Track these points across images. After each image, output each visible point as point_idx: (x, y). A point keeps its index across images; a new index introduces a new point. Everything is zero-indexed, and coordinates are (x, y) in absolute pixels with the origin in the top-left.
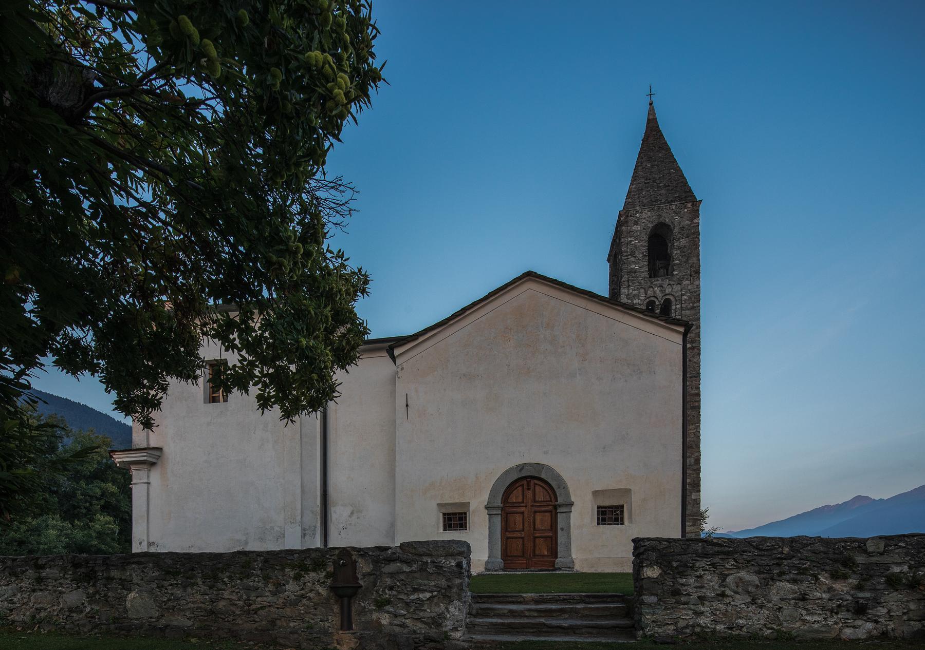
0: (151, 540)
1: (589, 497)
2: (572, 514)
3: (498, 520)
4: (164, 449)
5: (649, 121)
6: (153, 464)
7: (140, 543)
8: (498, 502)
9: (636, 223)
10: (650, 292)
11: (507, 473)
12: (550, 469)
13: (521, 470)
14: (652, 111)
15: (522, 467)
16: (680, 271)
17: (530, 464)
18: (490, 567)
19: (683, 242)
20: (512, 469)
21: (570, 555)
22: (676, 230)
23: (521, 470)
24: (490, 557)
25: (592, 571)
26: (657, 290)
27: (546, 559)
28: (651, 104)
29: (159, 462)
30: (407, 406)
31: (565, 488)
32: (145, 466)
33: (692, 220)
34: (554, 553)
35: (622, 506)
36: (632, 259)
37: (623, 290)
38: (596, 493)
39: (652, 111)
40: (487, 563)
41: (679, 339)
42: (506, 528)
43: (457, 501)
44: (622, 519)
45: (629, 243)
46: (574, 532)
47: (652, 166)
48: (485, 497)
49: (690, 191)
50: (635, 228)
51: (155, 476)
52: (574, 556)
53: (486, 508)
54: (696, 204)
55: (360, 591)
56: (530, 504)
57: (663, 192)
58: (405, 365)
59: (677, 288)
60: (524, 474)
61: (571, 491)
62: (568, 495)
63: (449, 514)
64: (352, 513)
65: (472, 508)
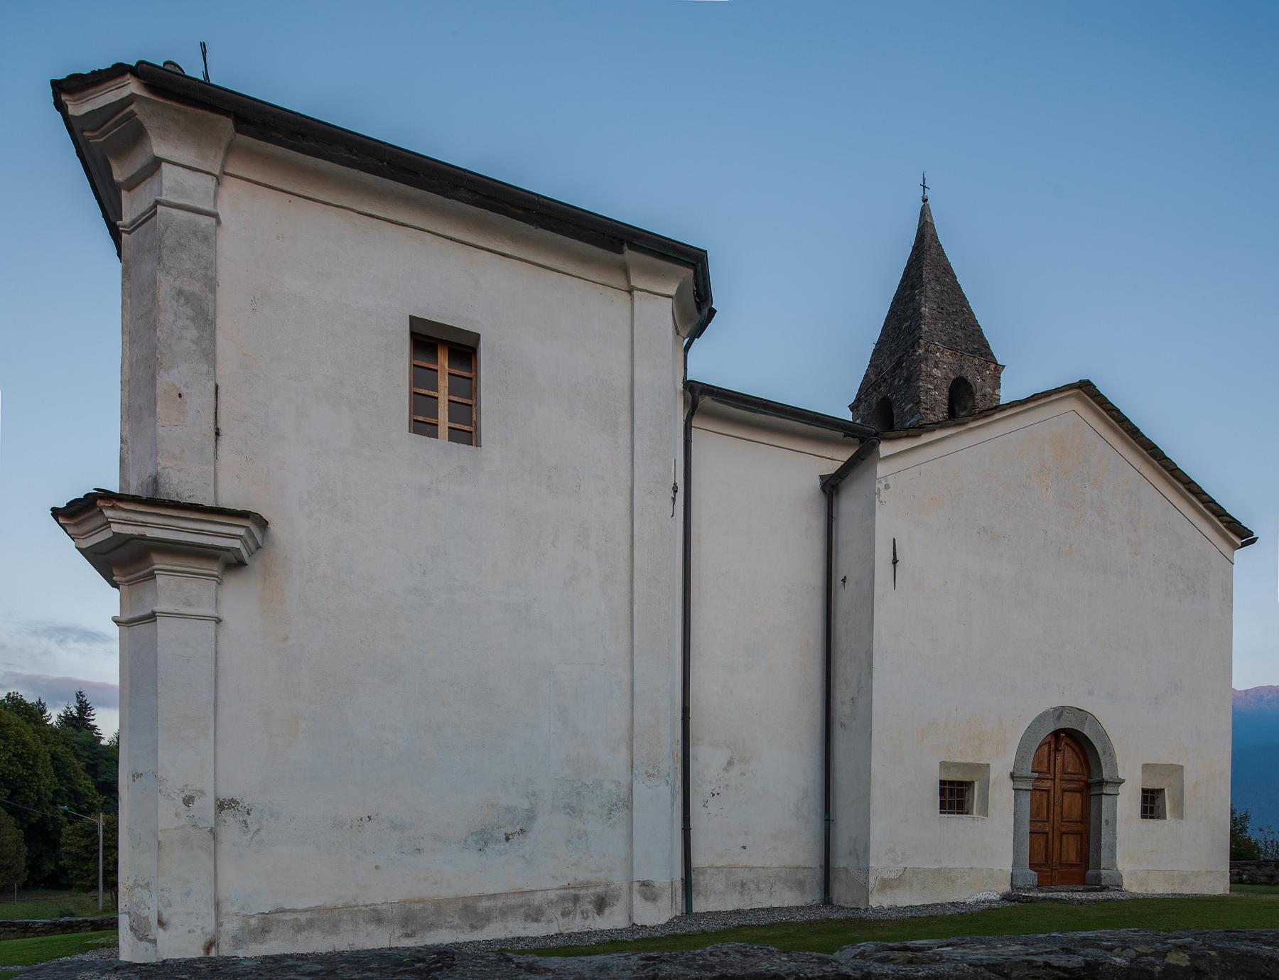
0: (226, 794)
2: (1119, 798)
6: (234, 564)
7: (188, 801)
8: (1027, 770)
11: (1040, 719)
13: (1059, 717)
14: (925, 212)
18: (1019, 883)
20: (1046, 713)
21: (1114, 865)
23: (1059, 717)
27: (1074, 869)
28: (925, 201)
29: (255, 564)
30: (895, 562)
32: (215, 569)
35: (970, 784)
38: (944, 765)
39: (925, 212)
43: (972, 761)
50: (935, 371)
51: (238, 600)
52: (1120, 867)
54: (999, 368)
55: (24, 878)
56: (1058, 775)
58: (891, 480)
61: (1118, 759)
63: (951, 783)
64: (730, 763)
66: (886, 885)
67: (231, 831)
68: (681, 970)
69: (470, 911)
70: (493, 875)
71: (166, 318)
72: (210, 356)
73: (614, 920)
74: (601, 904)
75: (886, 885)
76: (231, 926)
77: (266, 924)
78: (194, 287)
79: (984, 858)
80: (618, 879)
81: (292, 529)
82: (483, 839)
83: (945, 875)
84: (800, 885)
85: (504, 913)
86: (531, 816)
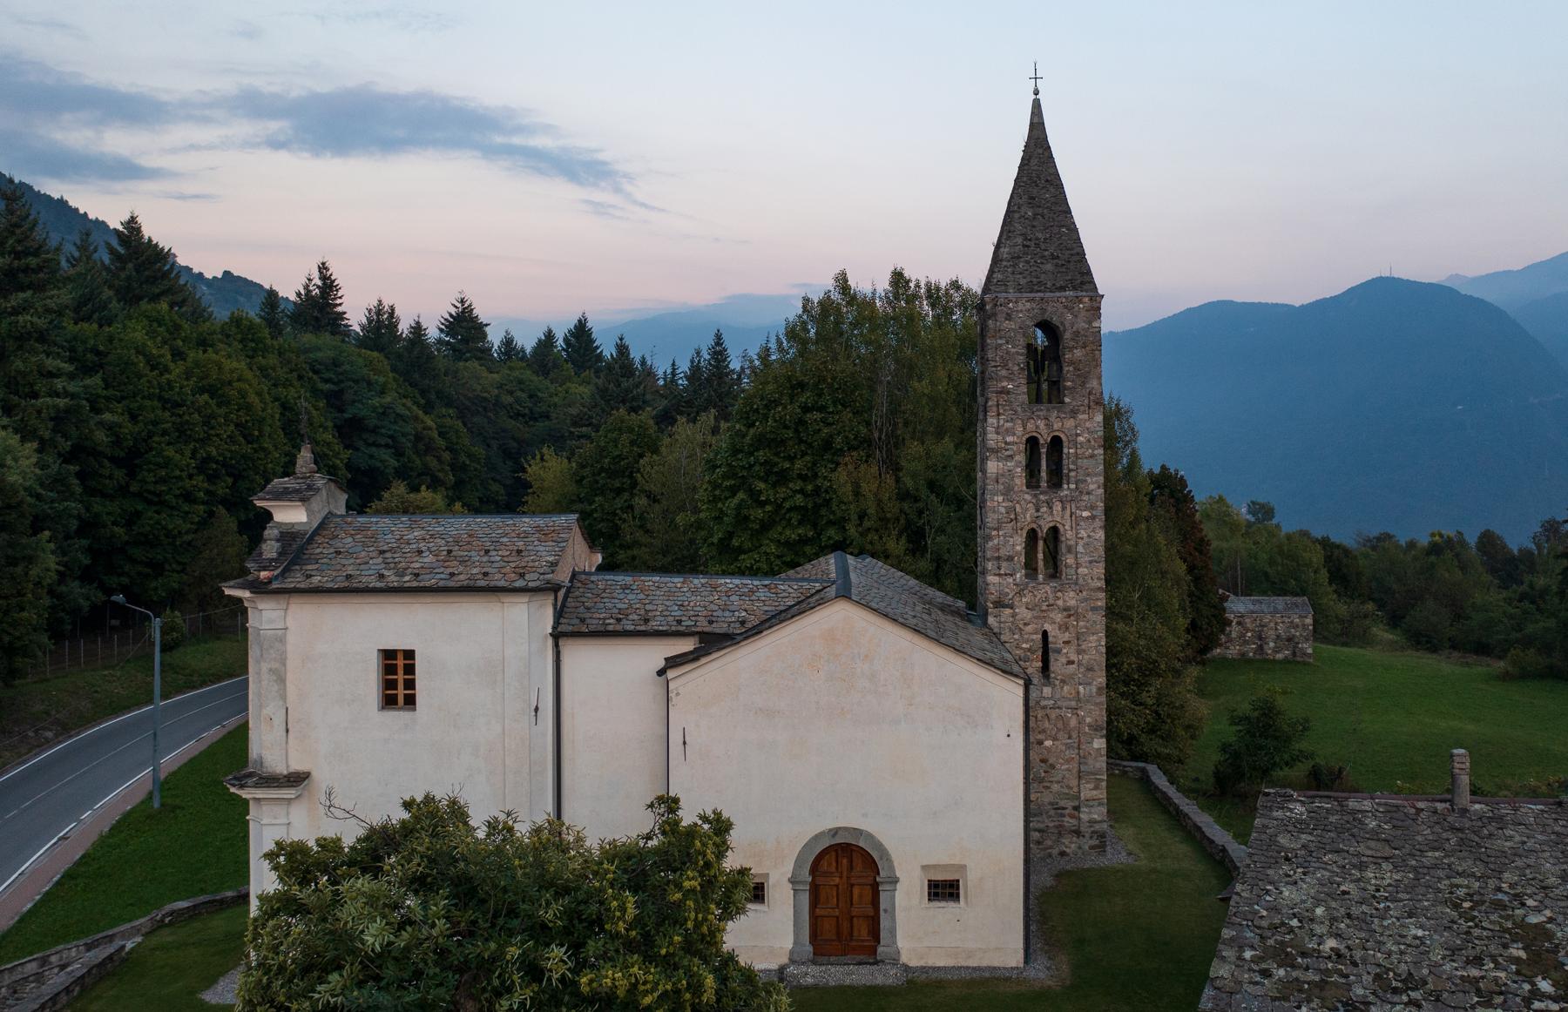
1: (918, 872)
3: (805, 898)
4: (314, 774)
5: (1032, 125)
9: (1009, 317)
10: (1030, 426)
11: (817, 838)
12: (870, 836)
13: (834, 836)
14: (1037, 106)
15: (835, 832)
16: (1073, 399)
17: (846, 829)
19: (1078, 353)
22: (1067, 335)
24: (795, 943)
25: (922, 963)
26: (1041, 423)
31: (889, 860)
33: (1090, 323)
34: (877, 938)
36: (1004, 373)
37: (990, 420)
38: (925, 868)
39: (1037, 106)
40: (792, 952)
41: (1020, 691)
42: (814, 903)
44: (958, 896)
45: (998, 347)
46: (900, 915)
47: (1035, 215)
48: (788, 868)
49: (1089, 273)
52: (900, 944)
53: (791, 881)
57: (1049, 267)
59: (1070, 423)
60: (838, 840)
62: (892, 868)
65: (772, 881)
81: (323, 776)
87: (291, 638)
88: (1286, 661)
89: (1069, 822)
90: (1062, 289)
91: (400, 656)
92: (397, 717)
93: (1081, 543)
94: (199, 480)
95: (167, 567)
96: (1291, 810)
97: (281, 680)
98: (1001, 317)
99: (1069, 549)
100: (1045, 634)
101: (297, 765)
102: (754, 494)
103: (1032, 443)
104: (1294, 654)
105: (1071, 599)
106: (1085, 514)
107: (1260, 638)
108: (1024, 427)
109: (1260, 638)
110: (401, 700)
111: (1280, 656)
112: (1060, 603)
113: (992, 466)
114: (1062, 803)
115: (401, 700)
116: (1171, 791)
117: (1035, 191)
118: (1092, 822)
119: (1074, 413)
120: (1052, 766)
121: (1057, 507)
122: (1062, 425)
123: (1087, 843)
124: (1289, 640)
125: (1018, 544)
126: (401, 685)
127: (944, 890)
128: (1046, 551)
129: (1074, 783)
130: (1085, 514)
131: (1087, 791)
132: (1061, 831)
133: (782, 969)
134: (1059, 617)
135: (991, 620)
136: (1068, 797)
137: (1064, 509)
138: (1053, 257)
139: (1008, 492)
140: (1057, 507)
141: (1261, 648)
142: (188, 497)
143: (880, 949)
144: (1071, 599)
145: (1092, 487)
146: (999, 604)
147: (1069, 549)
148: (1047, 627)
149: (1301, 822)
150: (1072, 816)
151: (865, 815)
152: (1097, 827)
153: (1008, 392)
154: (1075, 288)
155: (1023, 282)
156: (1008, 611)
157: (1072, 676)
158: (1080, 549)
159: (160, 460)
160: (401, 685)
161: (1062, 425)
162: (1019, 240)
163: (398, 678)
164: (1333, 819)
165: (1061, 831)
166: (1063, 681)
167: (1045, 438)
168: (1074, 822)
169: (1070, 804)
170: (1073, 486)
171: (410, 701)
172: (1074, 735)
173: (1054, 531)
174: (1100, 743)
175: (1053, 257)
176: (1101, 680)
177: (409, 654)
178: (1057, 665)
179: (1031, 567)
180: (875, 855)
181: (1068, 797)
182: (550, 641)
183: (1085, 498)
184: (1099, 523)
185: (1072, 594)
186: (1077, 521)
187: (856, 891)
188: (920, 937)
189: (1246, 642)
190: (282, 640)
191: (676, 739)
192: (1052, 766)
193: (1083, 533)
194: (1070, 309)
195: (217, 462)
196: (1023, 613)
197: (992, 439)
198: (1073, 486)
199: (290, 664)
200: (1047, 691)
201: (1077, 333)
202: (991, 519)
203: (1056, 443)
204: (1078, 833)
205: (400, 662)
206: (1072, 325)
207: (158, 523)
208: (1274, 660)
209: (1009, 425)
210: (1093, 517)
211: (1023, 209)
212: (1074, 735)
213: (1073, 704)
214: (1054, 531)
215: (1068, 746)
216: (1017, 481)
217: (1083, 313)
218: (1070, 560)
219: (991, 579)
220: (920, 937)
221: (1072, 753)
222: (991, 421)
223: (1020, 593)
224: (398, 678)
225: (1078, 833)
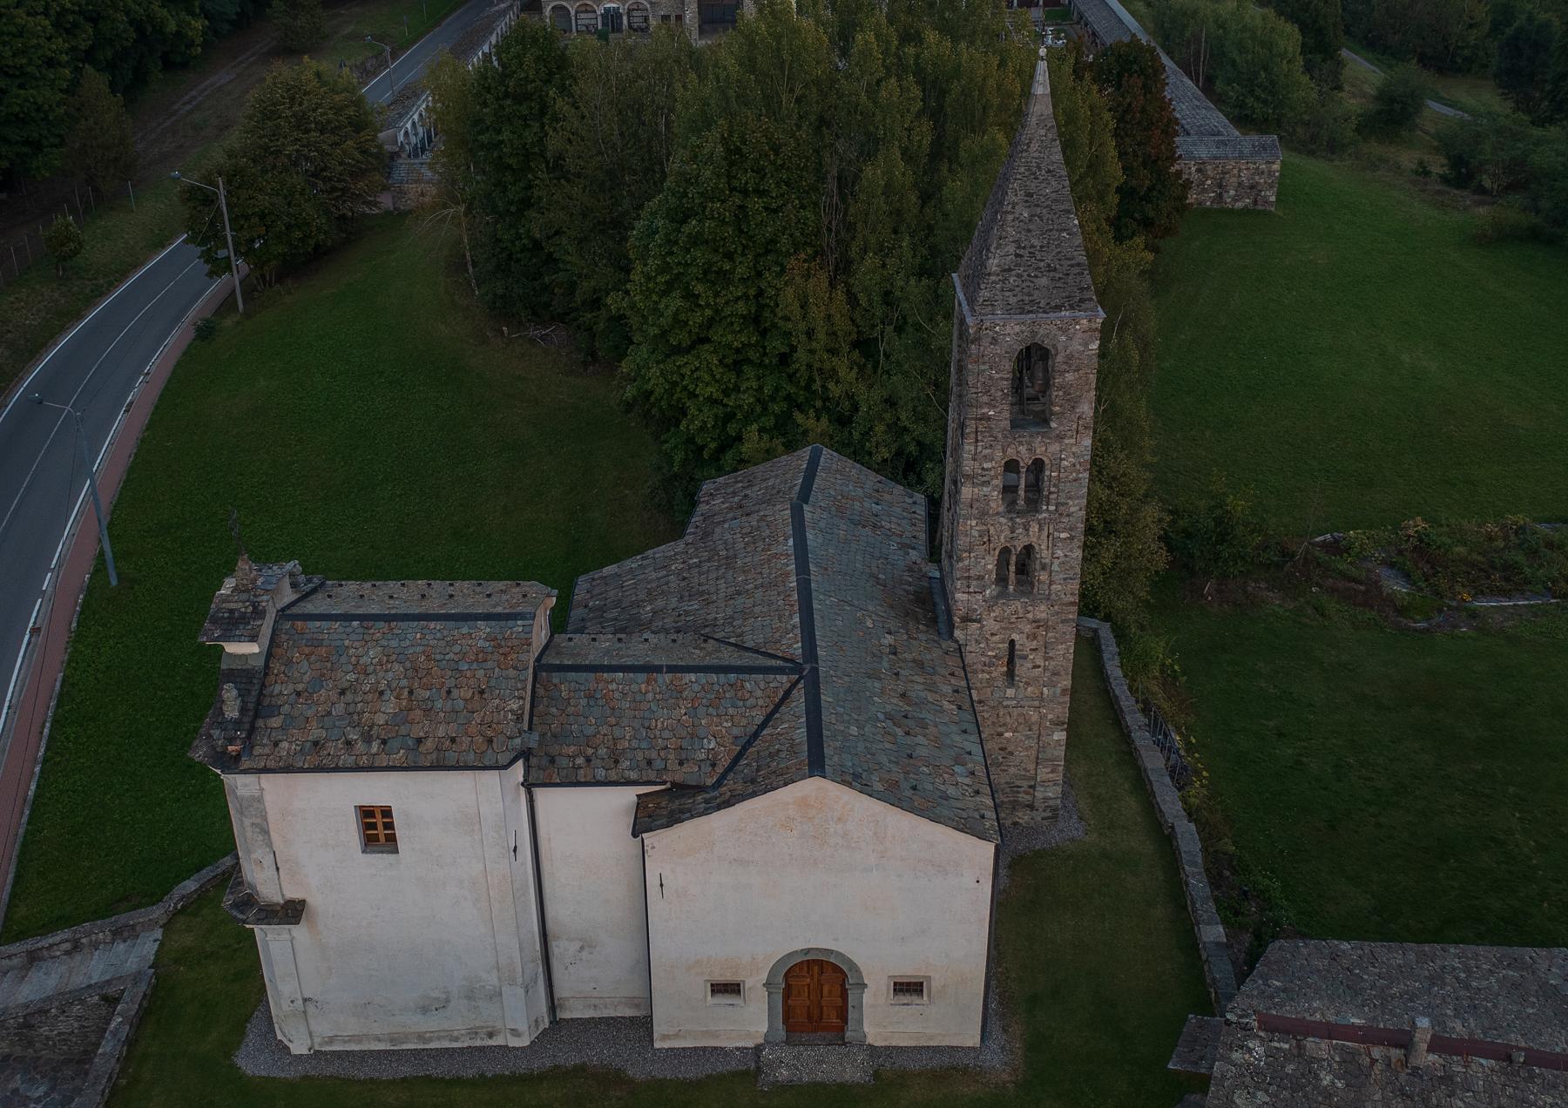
9: (994, 341)
16: (1061, 424)
19: (1070, 377)
22: (1060, 359)
36: (985, 399)
37: (967, 447)
51: (299, 931)
57: (1044, 281)
59: (1055, 447)
64: (582, 948)
66: (665, 1037)
67: (311, 1008)
68: (486, 48)
69: (421, 1037)
70: (431, 1024)
71: (249, 834)
72: (270, 845)
73: (498, 1041)
74: (491, 1035)
75: (665, 1037)
76: (317, 1040)
77: (331, 1040)
78: (258, 821)
79: (750, 1023)
80: (499, 1025)
81: (315, 900)
82: (425, 1010)
83: (714, 1035)
84: (637, 1006)
85: (439, 1038)
86: (448, 1001)
87: (268, 798)
88: (1246, 211)
89: (1024, 798)
90: (1058, 308)
91: (379, 815)
92: (380, 860)
93: (1056, 562)
94: (59, 43)
95: (45, 143)
96: (1250, 1051)
97: (265, 832)
98: (985, 342)
99: (1044, 567)
100: (1012, 643)
101: (292, 893)
102: (689, 296)
103: (1011, 466)
104: (1255, 202)
105: (1042, 611)
106: (1063, 535)
107: (1220, 186)
108: (1004, 451)
109: (1220, 186)
110: (382, 838)
111: (1239, 205)
112: (1030, 616)
113: (967, 492)
114: (1018, 783)
115: (382, 838)
116: (1127, 702)
117: (1032, 186)
118: (1046, 799)
119: (1060, 438)
120: (1011, 753)
121: (1035, 528)
122: (1044, 448)
123: (1039, 816)
124: (1252, 187)
125: (990, 564)
126: (380, 826)
127: (909, 988)
128: (1020, 568)
129: (1032, 766)
130: (1063, 535)
131: (1043, 773)
132: (1015, 805)
133: (758, 1049)
134: (1028, 628)
135: (957, 633)
136: (1024, 778)
137: (1041, 530)
138: (1050, 269)
139: (983, 515)
140: (1035, 528)
141: (1220, 196)
142: (51, 63)
143: (848, 1034)
144: (1042, 611)
145: (1073, 509)
146: (966, 619)
147: (1044, 567)
148: (1015, 636)
149: (1258, 1072)
150: (1027, 793)
151: (836, 940)
152: (1051, 803)
153: (989, 418)
154: (1072, 307)
155: (1012, 300)
156: (976, 625)
157: (1036, 679)
158: (1055, 567)
159: (12, 29)
160: (380, 826)
161: (1044, 448)
162: (1011, 249)
163: (377, 829)
164: (1289, 1069)
165: (1015, 805)
166: (1027, 684)
167: (1025, 459)
168: (1028, 797)
169: (1025, 784)
170: (1052, 508)
171: (392, 839)
172: (1035, 728)
173: (1029, 549)
174: (1060, 736)
175: (1050, 269)
176: (1066, 682)
177: (387, 812)
178: (1022, 669)
179: (1002, 580)
180: (845, 968)
181: (1024, 778)
182: (522, 790)
183: (1065, 520)
184: (1077, 543)
185: (1043, 607)
186: (1054, 542)
187: (826, 989)
188: (881, 1022)
189: (1204, 191)
190: (260, 800)
191: (652, 881)
192: (1011, 753)
193: (1059, 553)
194: (1064, 331)
195: (73, 12)
196: (990, 624)
197: (968, 466)
198: (1052, 508)
199: (271, 818)
200: (1010, 692)
201: (1070, 357)
202: (962, 541)
203: (1038, 465)
204: (1031, 807)
205: (379, 820)
206: (1066, 348)
207: (26, 100)
208: (1232, 211)
209: (986, 452)
210: (1072, 538)
211: (1018, 209)
212: (1035, 728)
213: (1036, 703)
214: (1029, 549)
215: (1028, 737)
216: (993, 505)
217: (1080, 335)
218: (1044, 576)
219: (958, 596)
220: (881, 1022)
221: (1033, 743)
222: (968, 448)
223: (990, 609)
224: (377, 829)
225: (1031, 807)
